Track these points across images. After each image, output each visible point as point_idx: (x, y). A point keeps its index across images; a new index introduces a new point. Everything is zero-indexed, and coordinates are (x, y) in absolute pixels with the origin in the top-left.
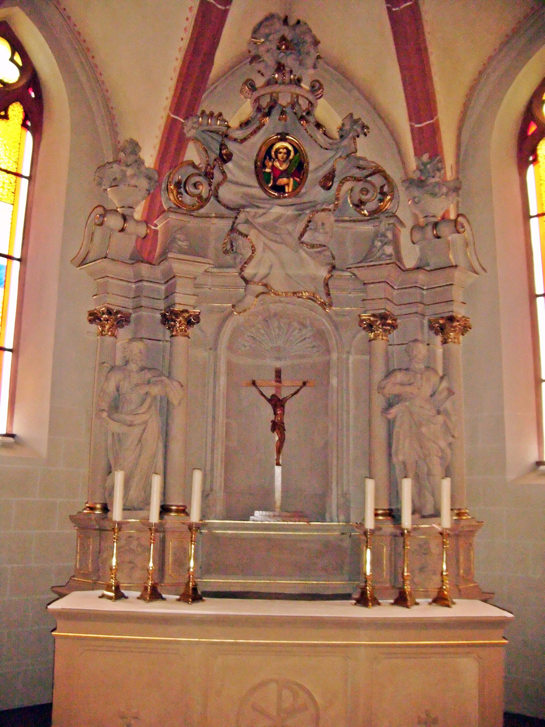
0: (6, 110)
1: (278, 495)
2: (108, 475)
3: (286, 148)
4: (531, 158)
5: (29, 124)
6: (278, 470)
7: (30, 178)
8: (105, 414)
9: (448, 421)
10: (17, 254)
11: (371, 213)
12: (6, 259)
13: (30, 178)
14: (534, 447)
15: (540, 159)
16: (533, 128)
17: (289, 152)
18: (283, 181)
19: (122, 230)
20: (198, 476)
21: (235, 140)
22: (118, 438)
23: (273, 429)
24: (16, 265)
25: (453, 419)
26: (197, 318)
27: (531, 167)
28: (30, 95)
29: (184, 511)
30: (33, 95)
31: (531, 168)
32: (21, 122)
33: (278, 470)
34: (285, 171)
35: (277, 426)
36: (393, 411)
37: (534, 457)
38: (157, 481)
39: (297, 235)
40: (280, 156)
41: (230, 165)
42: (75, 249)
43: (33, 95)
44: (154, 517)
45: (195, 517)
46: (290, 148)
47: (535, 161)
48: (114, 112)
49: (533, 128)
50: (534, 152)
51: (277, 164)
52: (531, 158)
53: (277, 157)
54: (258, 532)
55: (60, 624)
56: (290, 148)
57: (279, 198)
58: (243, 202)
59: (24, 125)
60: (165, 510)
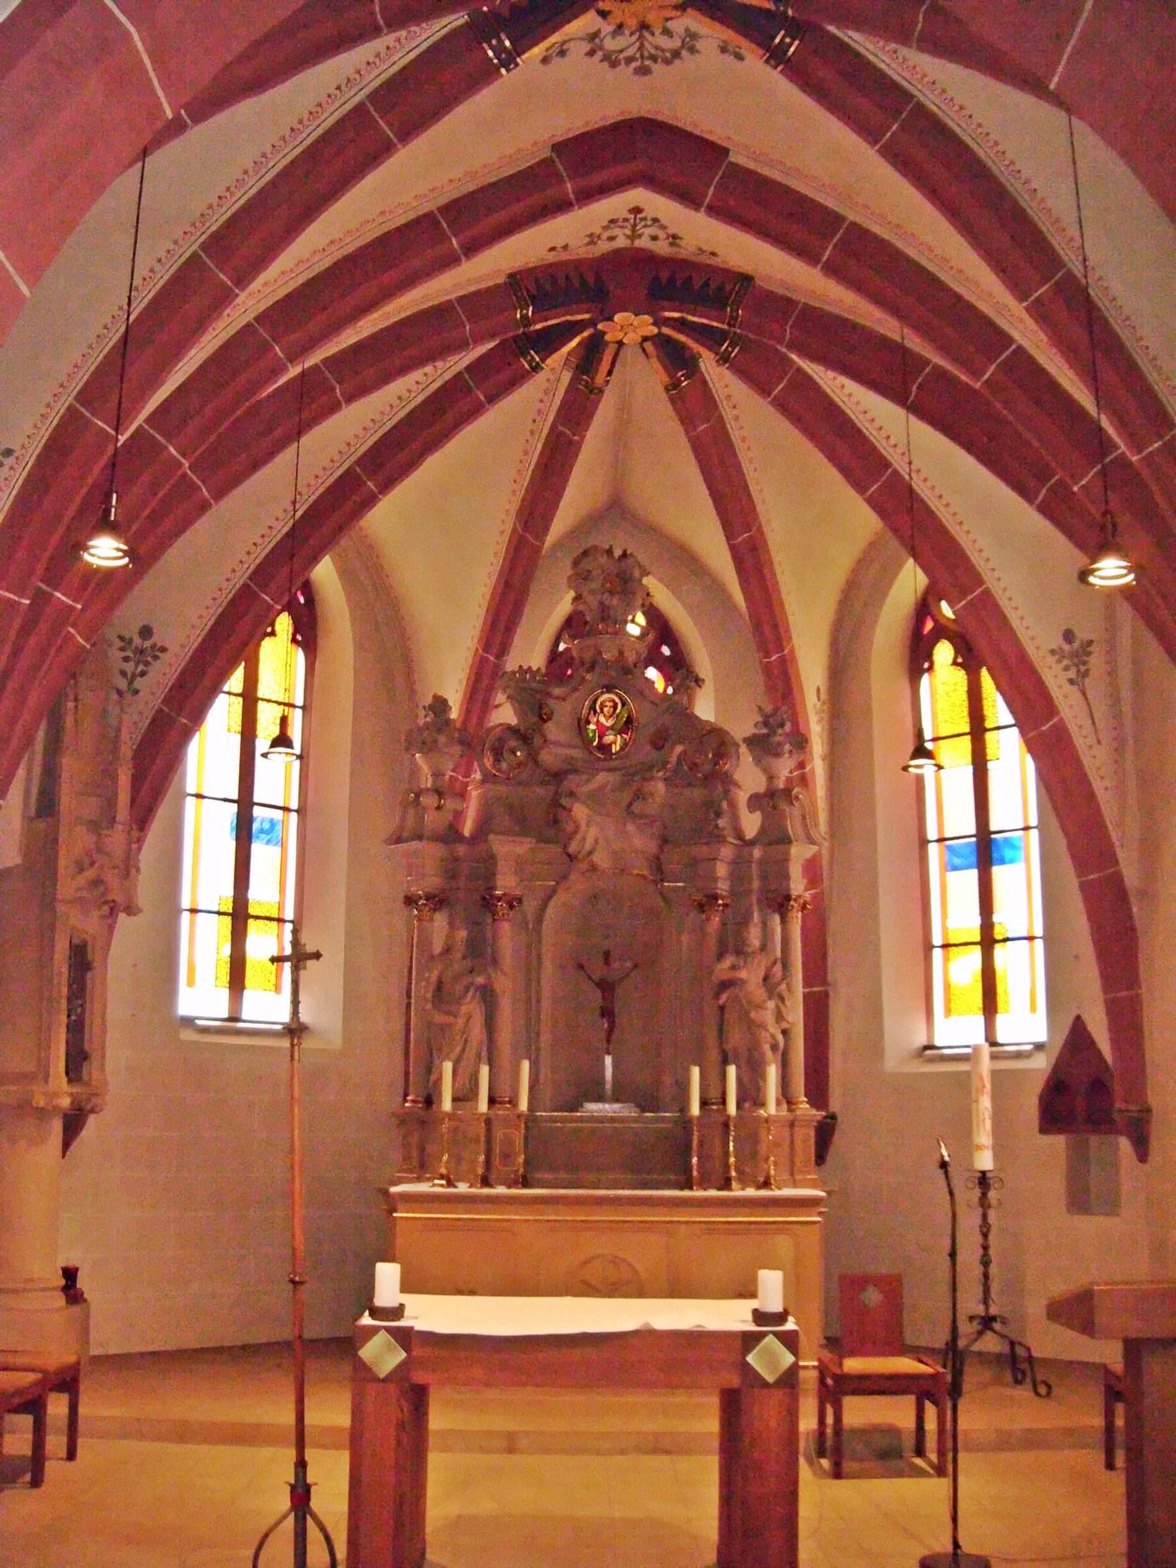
0: (273, 625)
1: (608, 1086)
2: (718, 960)
3: (613, 701)
4: (926, 665)
5: (299, 638)
6: (608, 1060)
7: (304, 708)
8: (429, 1006)
9: (781, 1005)
10: (294, 805)
11: (706, 777)
12: (281, 812)
13: (304, 708)
14: (922, 1027)
15: (936, 666)
16: (929, 625)
17: (615, 708)
18: (609, 738)
19: (439, 808)
20: (526, 1065)
21: (557, 698)
22: (444, 1028)
23: (603, 1015)
24: (294, 817)
25: (788, 1003)
26: (520, 901)
27: (926, 677)
28: (298, 600)
29: (513, 1102)
30: (302, 600)
31: (925, 677)
32: (290, 637)
33: (608, 1060)
34: (612, 728)
35: (607, 1012)
36: (724, 997)
37: (922, 1040)
38: (485, 1070)
39: (625, 803)
40: (606, 710)
41: (550, 724)
42: (388, 827)
43: (302, 600)
44: (483, 1106)
45: (523, 1105)
46: (617, 700)
47: (930, 669)
48: (403, 623)
49: (929, 625)
50: (929, 657)
51: (602, 719)
52: (926, 665)
53: (602, 712)
54: (155, 82)
55: (400, 1206)
56: (617, 700)
57: (605, 760)
58: (565, 766)
59: (294, 640)
60: (492, 1101)
